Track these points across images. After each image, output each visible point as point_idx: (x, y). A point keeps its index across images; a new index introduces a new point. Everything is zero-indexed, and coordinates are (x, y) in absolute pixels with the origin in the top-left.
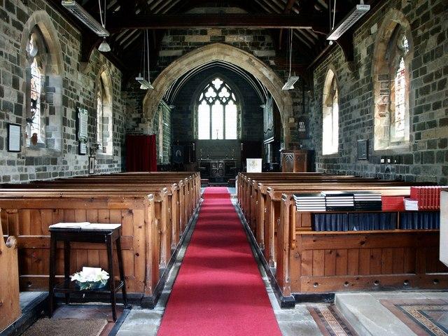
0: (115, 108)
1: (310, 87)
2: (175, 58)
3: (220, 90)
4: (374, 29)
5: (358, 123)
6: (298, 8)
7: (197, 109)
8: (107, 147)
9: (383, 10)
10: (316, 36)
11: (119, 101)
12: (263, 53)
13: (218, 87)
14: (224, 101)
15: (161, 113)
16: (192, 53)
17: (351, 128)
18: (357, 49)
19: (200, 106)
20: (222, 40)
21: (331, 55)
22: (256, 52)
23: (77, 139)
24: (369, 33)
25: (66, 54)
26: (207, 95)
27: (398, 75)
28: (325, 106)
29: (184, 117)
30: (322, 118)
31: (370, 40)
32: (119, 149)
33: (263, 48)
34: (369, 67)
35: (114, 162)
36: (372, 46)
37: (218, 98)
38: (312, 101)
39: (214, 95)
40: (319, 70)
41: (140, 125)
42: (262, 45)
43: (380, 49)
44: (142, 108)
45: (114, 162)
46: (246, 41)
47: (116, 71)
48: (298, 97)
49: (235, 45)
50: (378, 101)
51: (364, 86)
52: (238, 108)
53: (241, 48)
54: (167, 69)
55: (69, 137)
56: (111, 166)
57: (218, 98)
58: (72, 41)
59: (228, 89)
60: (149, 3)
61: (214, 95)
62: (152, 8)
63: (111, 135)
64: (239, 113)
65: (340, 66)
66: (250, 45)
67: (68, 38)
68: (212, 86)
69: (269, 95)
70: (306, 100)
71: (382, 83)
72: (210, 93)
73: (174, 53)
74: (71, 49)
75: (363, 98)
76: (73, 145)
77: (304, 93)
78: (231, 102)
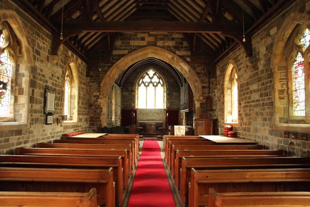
0: (80, 89)
1: (214, 76)
2: (123, 56)
3: (153, 77)
4: (273, 31)
5: (258, 103)
6: (211, 16)
7: (138, 89)
8: (73, 116)
9: (284, 15)
10: (223, 38)
11: (84, 84)
12: (182, 53)
13: (151, 75)
14: (155, 84)
15: (114, 92)
16: (134, 52)
17: (250, 106)
18: (255, 48)
19: (140, 88)
20: (155, 45)
21: (231, 54)
22: (177, 52)
23: (44, 113)
24: (268, 35)
25: (36, 48)
26: (145, 80)
27: (294, 66)
28: (226, 89)
29: (129, 94)
30: (224, 97)
31: (269, 41)
32: (84, 117)
33: (182, 49)
34: (269, 61)
35: (79, 127)
36: (272, 45)
37: (151, 82)
38: (216, 85)
39: (149, 80)
40: (221, 64)
41: (99, 100)
42: (182, 47)
43: (279, 48)
44: (100, 89)
45: (79, 127)
46: (171, 45)
47: (82, 63)
48: (205, 83)
49: (163, 47)
50: (278, 86)
51: (265, 75)
52: (164, 89)
53: (168, 50)
54: (118, 62)
55: (35, 111)
56: (76, 130)
57: (151, 82)
58: (43, 39)
59: (158, 77)
60: (101, 5)
61: (149, 80)
62: (105, 16)
63: (77, 107)
64: (164, 92)
65: (239, 61)
66: (173, 48)
67: (39, 36)
68: (148, 74)
69: (185, 81)
70: (211, 85)
71: (280, 73)
72: (146, 79)
73: (122, 52)
74: (41, 44)
75: (263, 84)
76: (40, 118)
77: (209, 80)
78: (159, 85)
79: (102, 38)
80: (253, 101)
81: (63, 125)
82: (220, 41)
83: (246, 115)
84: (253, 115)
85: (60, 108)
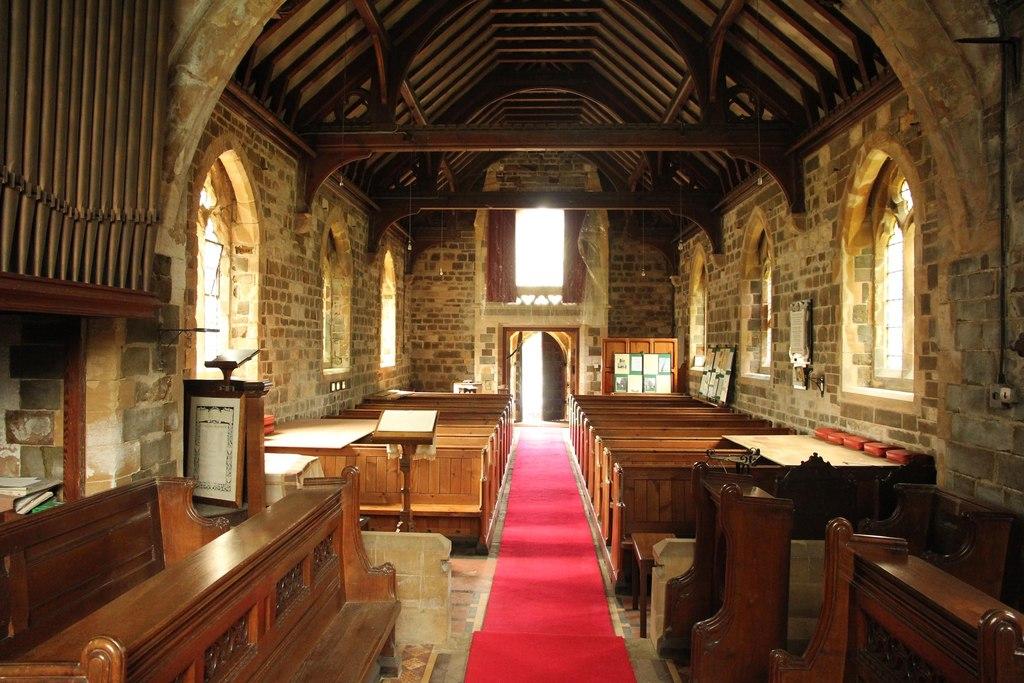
17: (289, 333)
79: (350, 69)
80: (293, 322)
81: (840, 399)
82: (826, 60)
83: (280, 356)
84: (294, 355)
85: (829, 343)
